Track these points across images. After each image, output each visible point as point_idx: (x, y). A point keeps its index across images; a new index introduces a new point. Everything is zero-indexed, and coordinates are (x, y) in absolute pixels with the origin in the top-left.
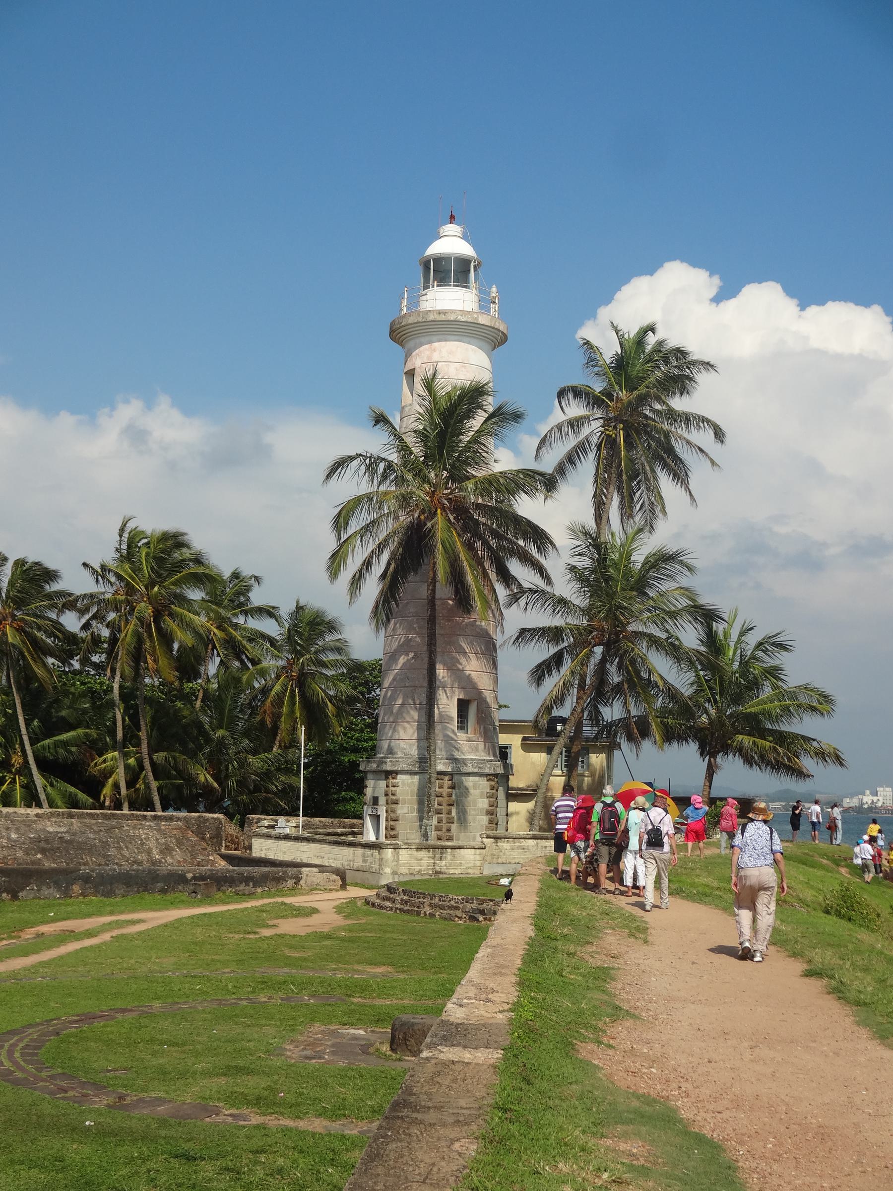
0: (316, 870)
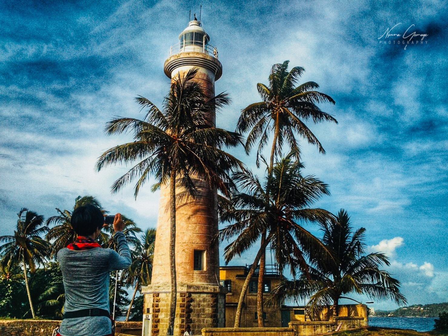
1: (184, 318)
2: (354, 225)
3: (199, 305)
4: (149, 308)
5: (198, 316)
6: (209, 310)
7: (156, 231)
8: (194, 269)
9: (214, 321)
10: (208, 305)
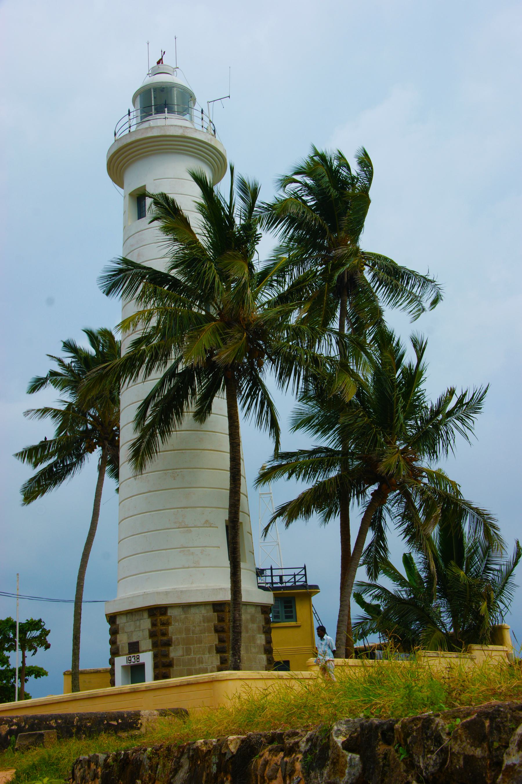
4: (134, 640)
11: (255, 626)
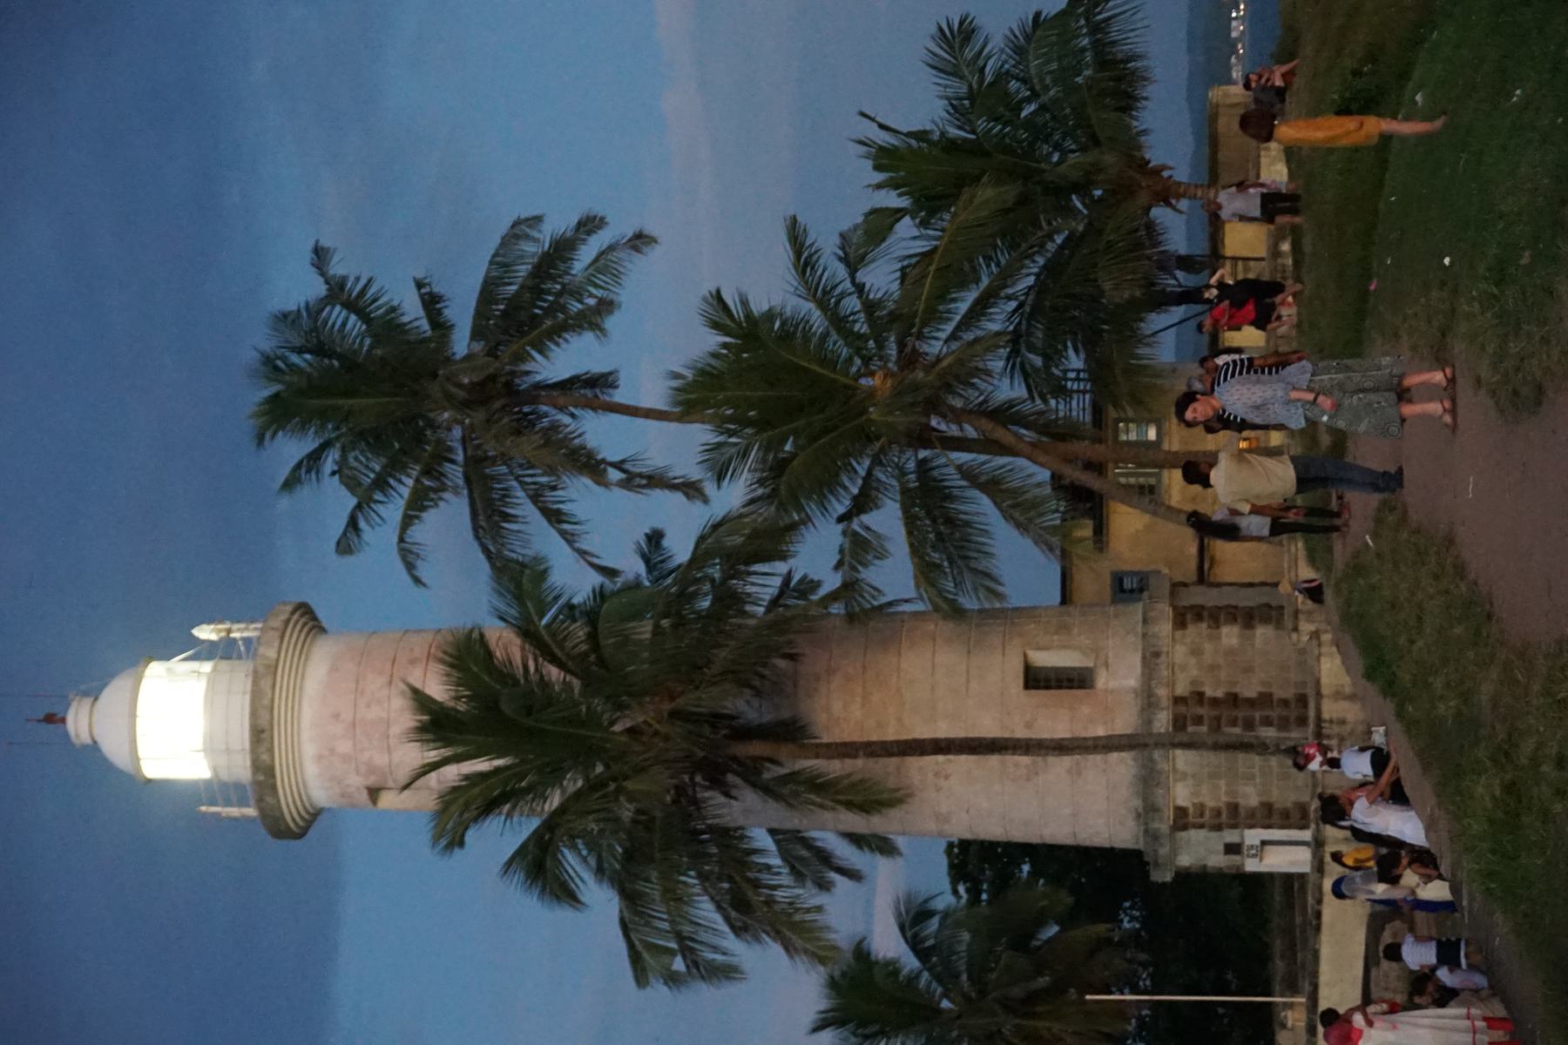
0: (1374, 972)
1: (1257, 715)
2: (922, 105)
3: (1214, 668)
4: (1221, 848)
5: (1249, 670)
6: (1230, 635)
7: (436, 840)
8: (1092, 687)
9: (1266, 620)
10: (1210, 638)
11: (1208, 647)
